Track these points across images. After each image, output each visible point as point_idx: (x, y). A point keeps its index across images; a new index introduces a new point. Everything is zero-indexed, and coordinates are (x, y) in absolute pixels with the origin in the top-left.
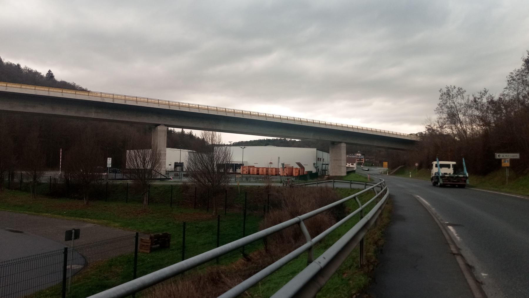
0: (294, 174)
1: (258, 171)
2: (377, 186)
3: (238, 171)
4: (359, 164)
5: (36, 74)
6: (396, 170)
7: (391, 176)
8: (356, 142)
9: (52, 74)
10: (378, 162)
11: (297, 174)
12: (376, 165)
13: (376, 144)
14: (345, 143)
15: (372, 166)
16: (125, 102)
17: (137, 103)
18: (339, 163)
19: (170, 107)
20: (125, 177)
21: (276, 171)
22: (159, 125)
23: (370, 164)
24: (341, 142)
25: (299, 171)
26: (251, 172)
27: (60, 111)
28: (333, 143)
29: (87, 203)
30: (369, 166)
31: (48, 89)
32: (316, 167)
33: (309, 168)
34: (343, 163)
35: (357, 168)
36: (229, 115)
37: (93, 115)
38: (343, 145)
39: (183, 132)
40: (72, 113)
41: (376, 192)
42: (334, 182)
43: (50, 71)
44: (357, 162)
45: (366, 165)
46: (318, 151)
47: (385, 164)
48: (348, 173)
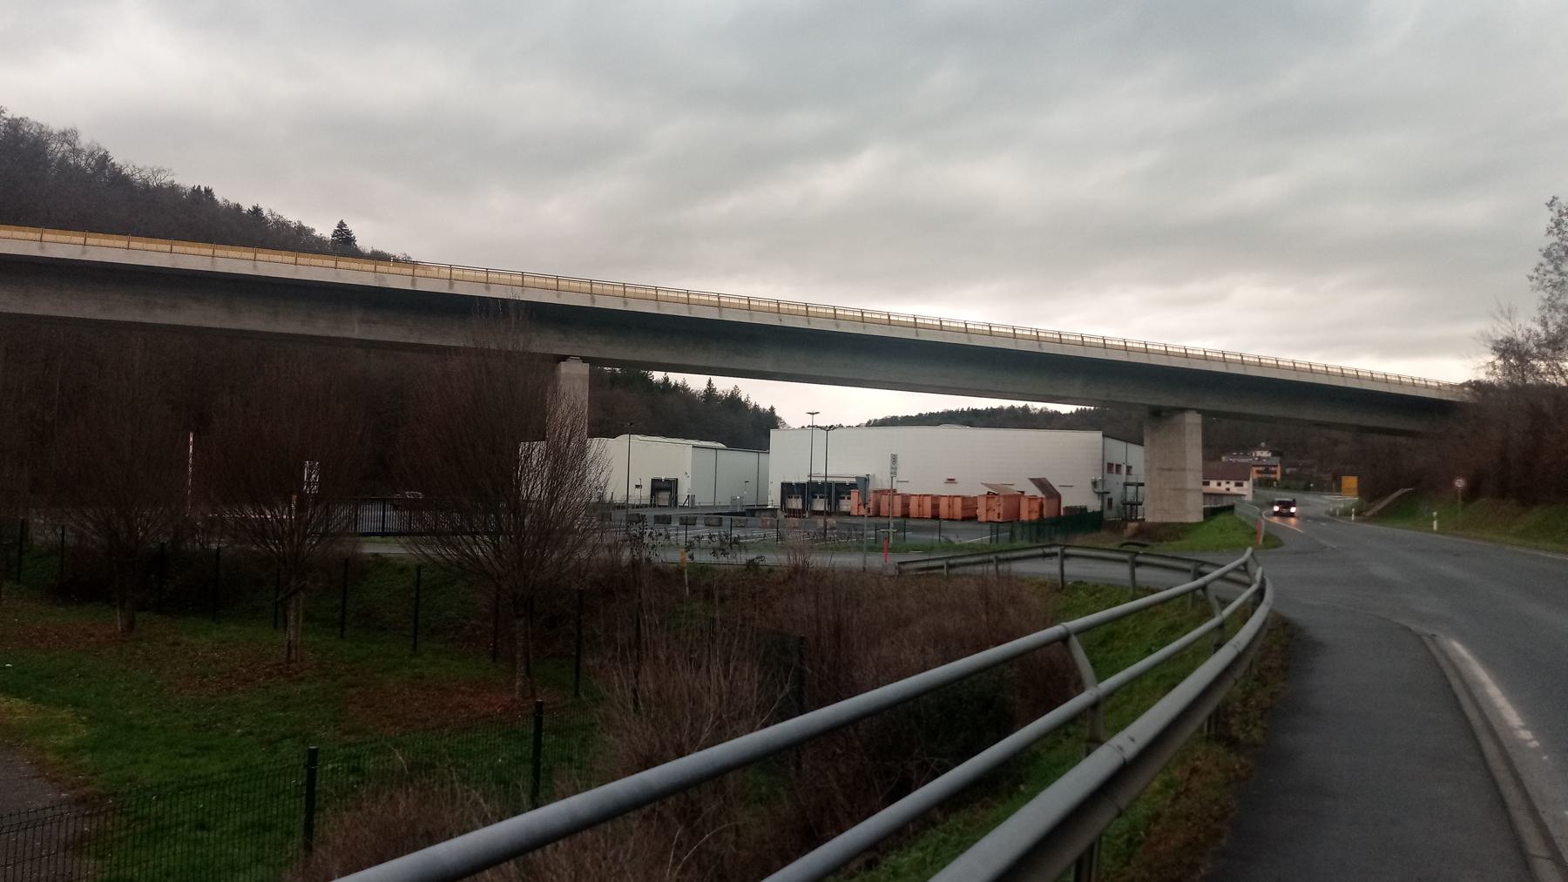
0: (1024, 516)
1: (906, 506)
2: (1222, 577)
3: (845, 505)
4: (1263, 483)
5: (302, 231)
6: (1385, 502)
7: (1366, 525)
8: (1237, 408)
9: (348, 233)
10: (1327, 477)
11: (1035, 517)
12: (1321, 488)
13: (1309, 414)
14: (1199, 411)
15: (1307, 489)
16: (451, 285)
17: (488, 289)
18: (1175, 479)
19: (593, 300)
20: (415, 526)
21: (964, 508)
22: (564, 358)
23: (1302, 484)
24: (1183, 410)
25: (1041, 507)
26: (884, 509)
27: (253, 320)
28: (1157, 414)
29: (131, 626)
30: (1296, 489)
31: (210, 252)
32: (1102, 495)
33: (1078, 495)
34: (1193, 480)
35: (1255, 495)
36: (788, 322)
37: (354, 328)
38: (1193, 420)
39: (667, 379)
40: (290, 324)
41: (1216, 604)
42: (1066, 556)
43: (342, 225)
44: (1254, 475)
45: (1287, 488)
46: (1108, 440)
47: (1350, 482)
48: (1210, 513)
